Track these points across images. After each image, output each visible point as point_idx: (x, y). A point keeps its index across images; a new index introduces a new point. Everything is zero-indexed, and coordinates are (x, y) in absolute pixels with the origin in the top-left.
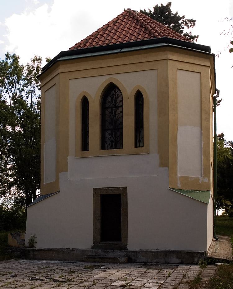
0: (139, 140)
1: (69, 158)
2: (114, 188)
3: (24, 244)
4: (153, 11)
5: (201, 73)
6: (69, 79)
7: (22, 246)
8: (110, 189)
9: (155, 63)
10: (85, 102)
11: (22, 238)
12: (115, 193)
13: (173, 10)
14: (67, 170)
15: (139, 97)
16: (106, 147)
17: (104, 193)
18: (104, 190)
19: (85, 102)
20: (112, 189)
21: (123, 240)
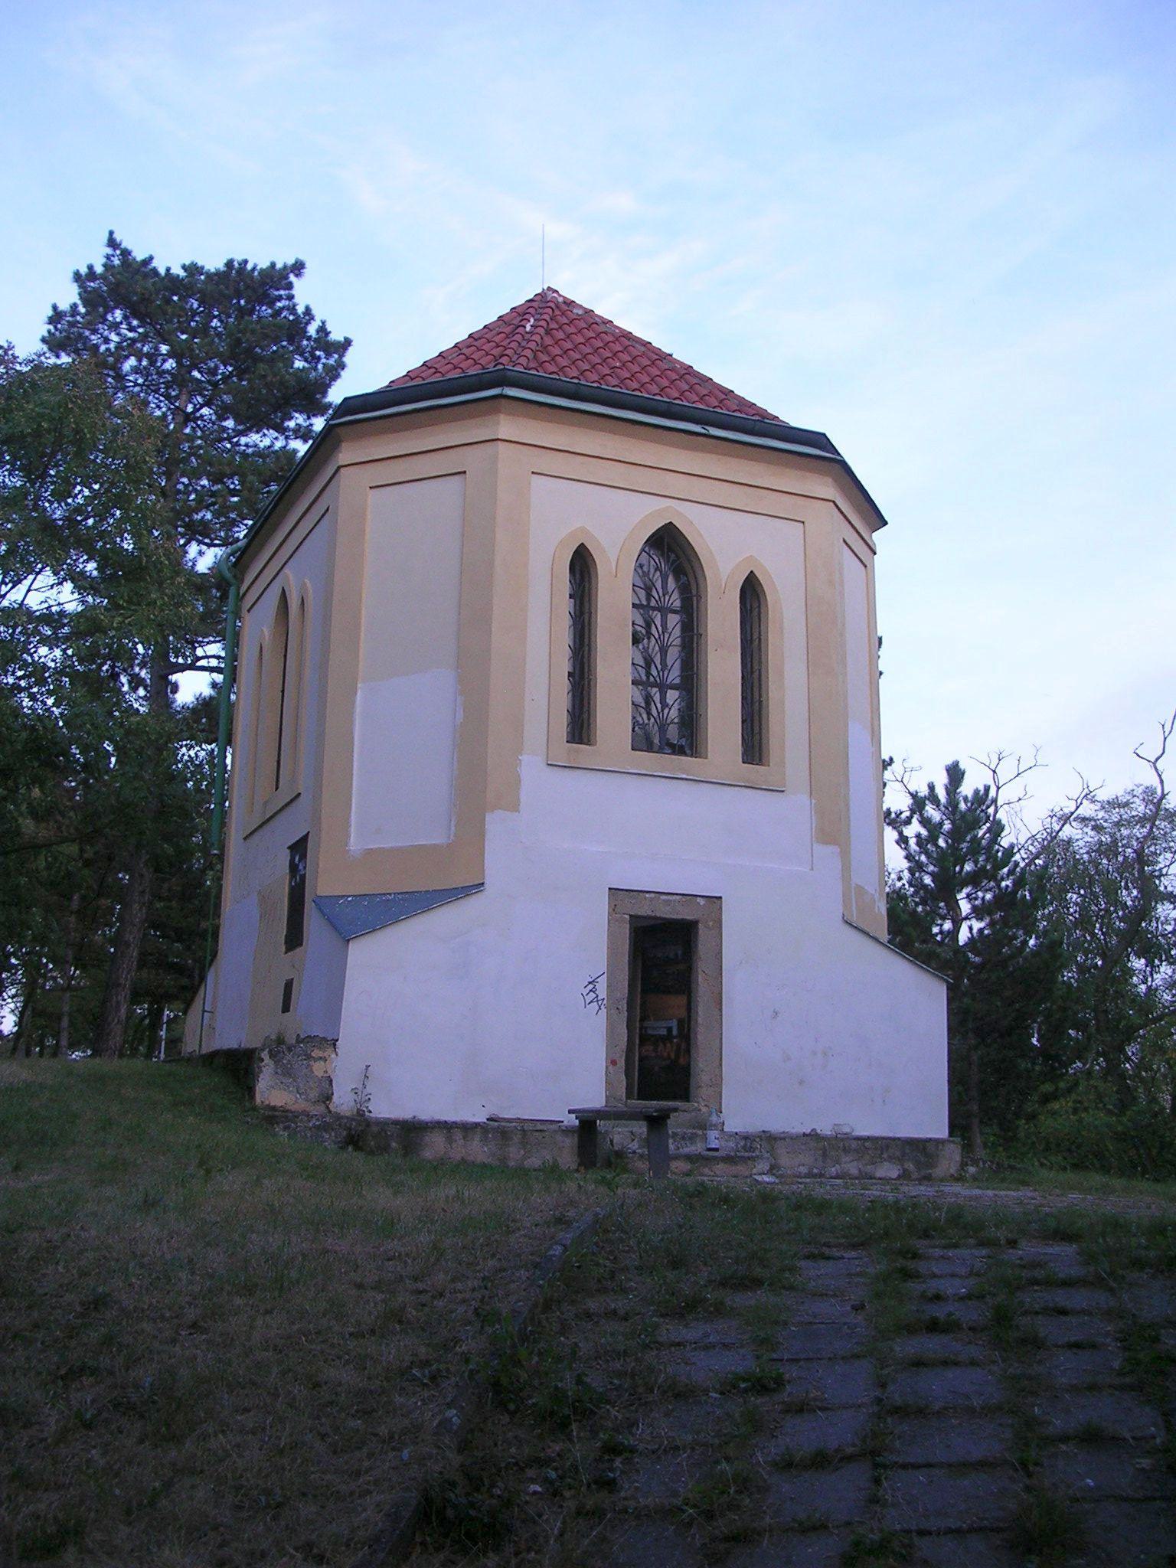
0: (754, 748)
1: (524, 758)
2: (678, 897)
3: (329, 1098)
4: (99, 269)
5: (803, 522)
6: (533, 473)
7: (322, 1108)
8: (664, 897)
9: (800, 501)
10: (582, 565)
11: (319, 1073)
12: (680, 917)
13: (304, 293)
14: (515, 807)
15: (752, 592)
16: (654, 750)
17: (642, 912)
18: (645, 898)
19: (582, 565)
20: (674, 897)
21: (704, 1092)
